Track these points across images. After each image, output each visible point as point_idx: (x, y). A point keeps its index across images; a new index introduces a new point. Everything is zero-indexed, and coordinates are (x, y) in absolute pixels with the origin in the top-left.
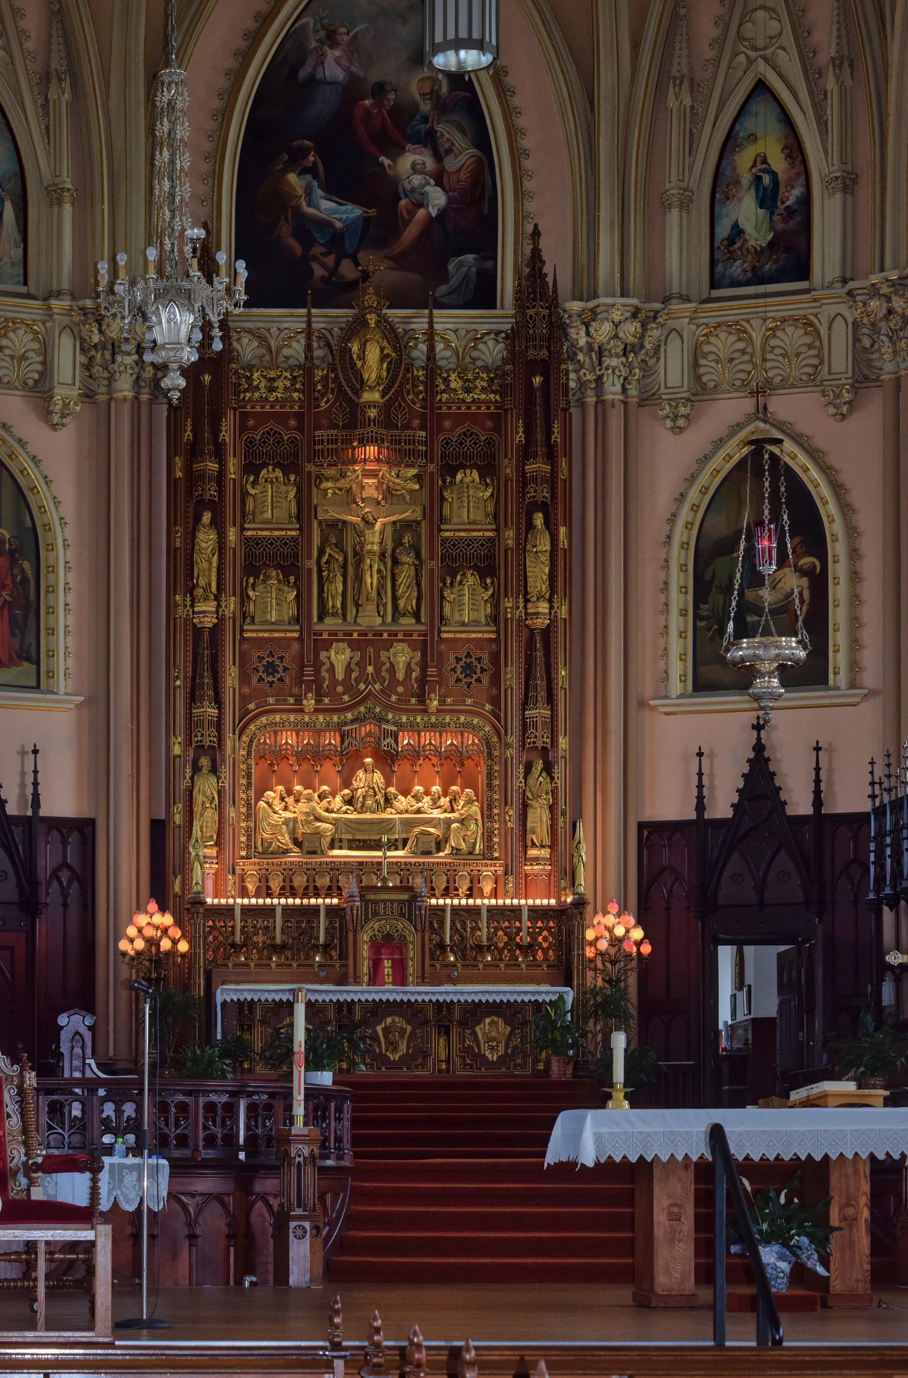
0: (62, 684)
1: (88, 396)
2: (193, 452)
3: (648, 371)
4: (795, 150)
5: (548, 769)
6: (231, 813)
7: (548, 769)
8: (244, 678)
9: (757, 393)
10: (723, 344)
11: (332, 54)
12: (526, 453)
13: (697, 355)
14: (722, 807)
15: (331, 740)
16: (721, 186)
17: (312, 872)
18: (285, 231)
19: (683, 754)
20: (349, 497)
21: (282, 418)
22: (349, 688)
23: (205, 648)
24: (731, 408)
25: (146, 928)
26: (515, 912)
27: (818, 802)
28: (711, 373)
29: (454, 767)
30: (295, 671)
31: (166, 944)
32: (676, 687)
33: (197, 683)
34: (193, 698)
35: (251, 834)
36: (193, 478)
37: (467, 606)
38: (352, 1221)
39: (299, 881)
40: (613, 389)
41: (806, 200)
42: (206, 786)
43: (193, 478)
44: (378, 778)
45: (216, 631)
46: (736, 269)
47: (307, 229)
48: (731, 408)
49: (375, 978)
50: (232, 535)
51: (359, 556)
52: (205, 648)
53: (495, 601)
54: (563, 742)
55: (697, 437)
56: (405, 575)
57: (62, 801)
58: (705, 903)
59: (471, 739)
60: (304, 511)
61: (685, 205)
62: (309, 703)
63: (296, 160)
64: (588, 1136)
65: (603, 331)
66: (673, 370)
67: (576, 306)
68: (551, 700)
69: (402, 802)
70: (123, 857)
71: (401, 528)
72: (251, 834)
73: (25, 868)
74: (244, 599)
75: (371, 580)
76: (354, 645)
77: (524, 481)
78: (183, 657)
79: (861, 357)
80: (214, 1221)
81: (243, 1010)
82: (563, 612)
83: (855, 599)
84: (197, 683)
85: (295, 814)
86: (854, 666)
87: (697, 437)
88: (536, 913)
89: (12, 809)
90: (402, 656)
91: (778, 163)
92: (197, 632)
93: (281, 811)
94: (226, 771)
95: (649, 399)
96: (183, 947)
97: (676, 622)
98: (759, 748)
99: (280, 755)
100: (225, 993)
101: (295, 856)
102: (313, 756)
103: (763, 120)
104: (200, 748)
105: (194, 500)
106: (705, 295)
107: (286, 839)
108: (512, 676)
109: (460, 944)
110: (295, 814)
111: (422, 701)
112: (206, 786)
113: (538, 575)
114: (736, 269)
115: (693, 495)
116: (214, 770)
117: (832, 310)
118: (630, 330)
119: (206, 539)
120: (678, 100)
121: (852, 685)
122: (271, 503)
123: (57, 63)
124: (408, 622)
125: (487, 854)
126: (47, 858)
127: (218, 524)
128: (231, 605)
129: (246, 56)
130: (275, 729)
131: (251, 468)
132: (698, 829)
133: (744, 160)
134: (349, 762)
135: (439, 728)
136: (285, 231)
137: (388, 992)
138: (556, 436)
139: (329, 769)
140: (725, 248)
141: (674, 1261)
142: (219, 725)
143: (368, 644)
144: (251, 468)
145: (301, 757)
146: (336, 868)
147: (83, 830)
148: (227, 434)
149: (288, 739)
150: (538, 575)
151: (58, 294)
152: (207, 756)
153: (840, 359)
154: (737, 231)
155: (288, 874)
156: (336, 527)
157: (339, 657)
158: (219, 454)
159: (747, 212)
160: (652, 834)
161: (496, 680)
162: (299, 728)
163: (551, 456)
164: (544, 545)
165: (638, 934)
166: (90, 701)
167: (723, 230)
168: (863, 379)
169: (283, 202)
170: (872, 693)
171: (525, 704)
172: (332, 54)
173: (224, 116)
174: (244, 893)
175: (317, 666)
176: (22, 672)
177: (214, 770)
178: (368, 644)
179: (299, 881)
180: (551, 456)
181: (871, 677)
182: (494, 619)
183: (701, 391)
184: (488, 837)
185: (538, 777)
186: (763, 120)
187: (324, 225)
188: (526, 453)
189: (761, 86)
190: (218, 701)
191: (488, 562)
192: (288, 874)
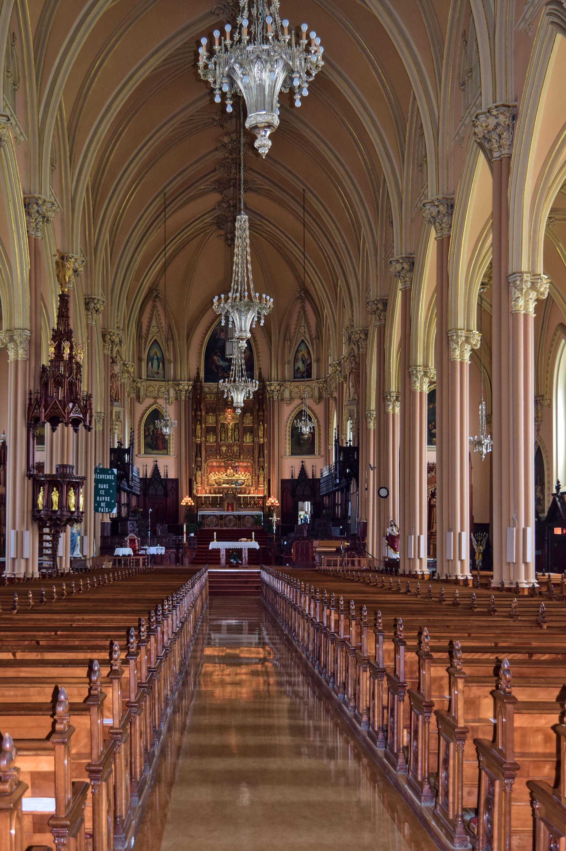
0: (172, 453)
1: (176, 399)
2: (196, 411)
3: (282, 394)
4: (309, 353)
5: (263, 470)
6: (204, 478)
7: (263, 470)
8: (206, 453)
9: (302, 399)
10: (296, 390)
11: (222, 334)
12: (258, 411)
13: (291, 392)
14: (296, 478)
15: (223, 464)
16: (296, 360)
17: (219, 489)
18: (214, 367)
19: (290, 466)
20: (226, 419)
21: (213, 404)
22: (226, 454)
23: (199, 447)
24: (297, 402)
25: (186, 501)
26: (254, 497)
27: (313, 476)
28: (293, 395)
29: (246, 469)
30: (216, 451)
31: (189, 504)
32: (288, 454)
33: (195, 456)
34: (196, 457)
35: (208, 482)
36: (196, 415)
37: (248, 439)
38: (196, 555)
39: (217, 491)
40: (275, 397)
41: (311, 363)
42: (199, 473)
43: (196, 415)
44: (232, 471)
45: (201, 444)
46: (298, 375)
47: (217, 367)
48: (297, 402)
49: (228, 510)
50: (203, 426)
51: (227, 429)
52: (199, 447)
53: (253, 438)
54: (266, 465)
55: (291, 407)
56: (236, 433)
57: (172, 475)
58: (293, 495)
59: (249, 464)
60: (217, 421)
61: (289, 363)
62: (218, 457)
63: (216, 354)
64: (213, 545)
65: (273, 388)
66: (287, 395)
67: (268, 383)
68: (263, 457)
69: (237, 475)
70: (184, 487)
71: (235, 424)
72: (208, 482)
73: (165, 488)
74: (206, 438)
75: (230, 434)
76: (227, 446)
77: (258, 416)
78: (194, 449)
79: (320, 393)
80: (173, 556)
81: (203, 516)
82: (266, 440)
83: (319, 438)
84: (195, 456)
85: (215, 478)
86: (319, 451)
87: (291, 407)
88: (258, 497)
89: (162, 477)
90: (236, 448)
91: (306, 356)
92: (197, 444)
93: (213, 477)
94: (203, 470)
95: (282, 399)
96: (193, 504)
97: (287, 442)
98: (303, 466)
99: (213, 467)
100: (200, 513)
101: (216, 486)
102: (219, 467)
103: (303, 347)
104: (198, 466)
105: (196, 419)
106: (293, 379)
107: (214, 483)
108: (256, 452)
109: (247, 503)
110: (215, 478)
111: (239, 456)
112: (199, 473)
113: (261, 433)
114: (298, 375)
115: (291, 418)
116: (200, 470)
117: (314, 385)
118: (278, 387)
119: (198, 427)
120: (287, 343)
121: (319, 454)
122: (211, 420)
123: (170, 337)
124: (237, 442)
125: (252, 486)
126: (169, 486)
127: (201, 424)
128: (203, 439)
129: (204, 338)
130: (212, 462)
131: (207, 413)
132: (292, 481)
133: (300, 355)
134: (226, 468)
135: (243, 462)
136: (214, 367)
137: (230, 513)
138: (264, 408)
139: (223, 469)
140: (296, 371)
141: (223, 560)
142: (201, 462)
143: (229, 446)
144: (207, 413)
145: (217, 467)
146: (224, 488)
147: (176, 481)
148: (202, 407)
149: (215, 464)
150: (261, 433)
151: (170, 380)
152: (199, 468)
153: (316, 394)
154: (299, 368)
155: (215, 489)
156: (223, 424)
157: (224, 449)
158: (201, 411)
159: (300, 364)
160: (284, 482)
161: (253, 453)
162: (217, 462)
163: (263, 411)
164: (262, 428)
165: (277, 502)
166: (177, 456)
167: (296, 368)
168: (320, 398)
169: (213, 362)
170: (322, 456)
171: (259, 458)
172: (222, 334)
173: (201, 346)
174: (206, 493)
175: (220, 450)
176: (164, 451)
177: (200, 470)
178: (229, 446)
179: (217, 491)
180: (263, 411)
181: (322, 453)
182: (253, 441)
183: (292, 399)
184: (252, 482)
185: (261, 472)
186: (303, 347)
187: (221, 366)
188: (258, 411)
189: (303, 341)
190: (201, 457)
191: (252, 431)
192: (215, 489)
